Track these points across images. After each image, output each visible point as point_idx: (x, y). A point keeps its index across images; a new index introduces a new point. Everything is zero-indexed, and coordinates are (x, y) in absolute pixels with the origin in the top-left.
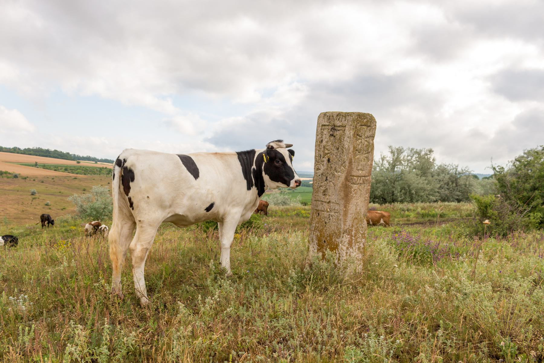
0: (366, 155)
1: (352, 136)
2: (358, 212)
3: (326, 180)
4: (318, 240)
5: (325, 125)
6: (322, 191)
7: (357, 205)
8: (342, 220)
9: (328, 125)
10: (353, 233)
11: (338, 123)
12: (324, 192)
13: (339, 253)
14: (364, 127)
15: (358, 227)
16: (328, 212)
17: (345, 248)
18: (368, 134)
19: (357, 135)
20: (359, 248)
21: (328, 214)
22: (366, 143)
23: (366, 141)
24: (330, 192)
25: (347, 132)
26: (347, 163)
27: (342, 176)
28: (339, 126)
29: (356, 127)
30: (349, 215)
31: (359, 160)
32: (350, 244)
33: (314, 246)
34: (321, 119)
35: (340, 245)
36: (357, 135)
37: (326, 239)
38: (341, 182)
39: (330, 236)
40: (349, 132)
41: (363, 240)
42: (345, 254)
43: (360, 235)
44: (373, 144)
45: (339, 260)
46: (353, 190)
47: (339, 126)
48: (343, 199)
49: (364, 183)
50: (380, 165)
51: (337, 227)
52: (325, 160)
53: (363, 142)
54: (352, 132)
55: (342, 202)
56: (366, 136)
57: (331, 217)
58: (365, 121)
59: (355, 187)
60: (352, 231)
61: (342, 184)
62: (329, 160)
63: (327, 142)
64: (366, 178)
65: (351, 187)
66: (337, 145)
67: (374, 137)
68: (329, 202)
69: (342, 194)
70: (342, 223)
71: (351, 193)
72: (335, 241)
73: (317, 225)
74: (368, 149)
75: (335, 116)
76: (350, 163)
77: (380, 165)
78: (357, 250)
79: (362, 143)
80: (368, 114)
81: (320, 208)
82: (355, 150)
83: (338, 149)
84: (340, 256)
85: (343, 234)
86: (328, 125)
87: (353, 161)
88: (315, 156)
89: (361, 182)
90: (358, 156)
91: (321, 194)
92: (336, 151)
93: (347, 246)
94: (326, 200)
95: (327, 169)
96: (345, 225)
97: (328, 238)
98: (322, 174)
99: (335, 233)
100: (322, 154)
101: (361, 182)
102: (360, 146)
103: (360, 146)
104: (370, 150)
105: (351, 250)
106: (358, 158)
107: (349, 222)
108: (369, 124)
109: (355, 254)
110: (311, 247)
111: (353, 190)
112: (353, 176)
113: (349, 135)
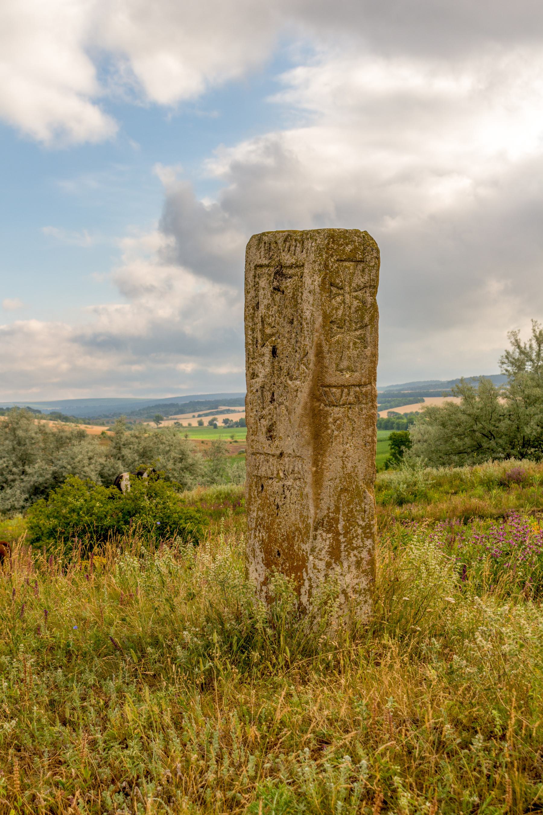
0: (358, 333)
1: (318, 290)
2: (349, 475)
3: (272, 400)
4: (266, 552)
5: (261, 266)
6: (264, 430)
7: (344, 458)
8: (311, 496)
9: (268, 266)
10: (340, 527)
11: (287, 259)
12: (269, 430)
13: (310, 579)
14: (347, 264)
15: (351, 511)
16: (281, 479)
17: (321, 565)
18: (359, 280)
19: (332, 285)
20: (358, 563)
21: (281, 483)
22: (356, 303)
23: (356, 298)
24: (281, 429)
25: (307, 280)
26: (312, 357)
27: (303, 387)
28: (291, 267)
29: (326, 266)
30: (326, 483)
31: (342, 347)
32: (335, 554)
33: (258, 567)
34: (253, 250)
35: (311, 558)
36: (330, 285)
37: (281, 546)
38: (302, 404)
39: (289, 539)
40: (312, 281)
41: (368, 542)
42: (322, 579)
43: (360, 531)
44: (374, 306)
45: (310, 595)
46: (330, 420)
47: (291, 267)
48: (309, 444)
49: (360, 403)
50: (534, 356)
51: (301, 516)
52: (267, 350)
53: (347, 301)
54: (318, 279)
55: (308, 453)
56: (354, 285)
57: (287, 493)
58: (349, 248)
59: (337, 412)
60: (337, 521)
61: (305, 408)
62: (274, 352)
63: (268, 307)
64: (364, 390)
65: (327, 415)
66: (288, 312)
67: (375, 287)
68: (281, 454)
69: (307, 432)
70: (311, 503)
71: (327, 428)
72: (299, 549)
73: (261, 514)
74: (362, 318)
75: (280, 242)
76: (319, 354)
77: (534, 356)
78: (353, 569)
79: (346, 302)
80: (356, 232)
81: (262, 472)
82: (329, 321)
83: (292, 322)
84: (311, 587)
85: (316, 529)
86: (268, 266)
87: (326, 349)
88: (247, 344)
89: (351, 399)
90: (336, 338)
91: (262, 437)
92: (288, 328)
93: (327, 559)
94: (273, 451)
95: (272, 374)
96: (317, 507)
97: (285, 545)
98: (263, 387)
99: (298, 529)
100: (259, 335)
101: (351, 399)
102: (340, 312)
103: (340, 312)
104: (367, 319)
105: (338, 569)
106: (338, 342)
107: (328, 501)
108: (359, 256)
109: (348, 577)
110: (251, 569)
111: (330, 420)
112: (329, 386)
113: (312, 287)
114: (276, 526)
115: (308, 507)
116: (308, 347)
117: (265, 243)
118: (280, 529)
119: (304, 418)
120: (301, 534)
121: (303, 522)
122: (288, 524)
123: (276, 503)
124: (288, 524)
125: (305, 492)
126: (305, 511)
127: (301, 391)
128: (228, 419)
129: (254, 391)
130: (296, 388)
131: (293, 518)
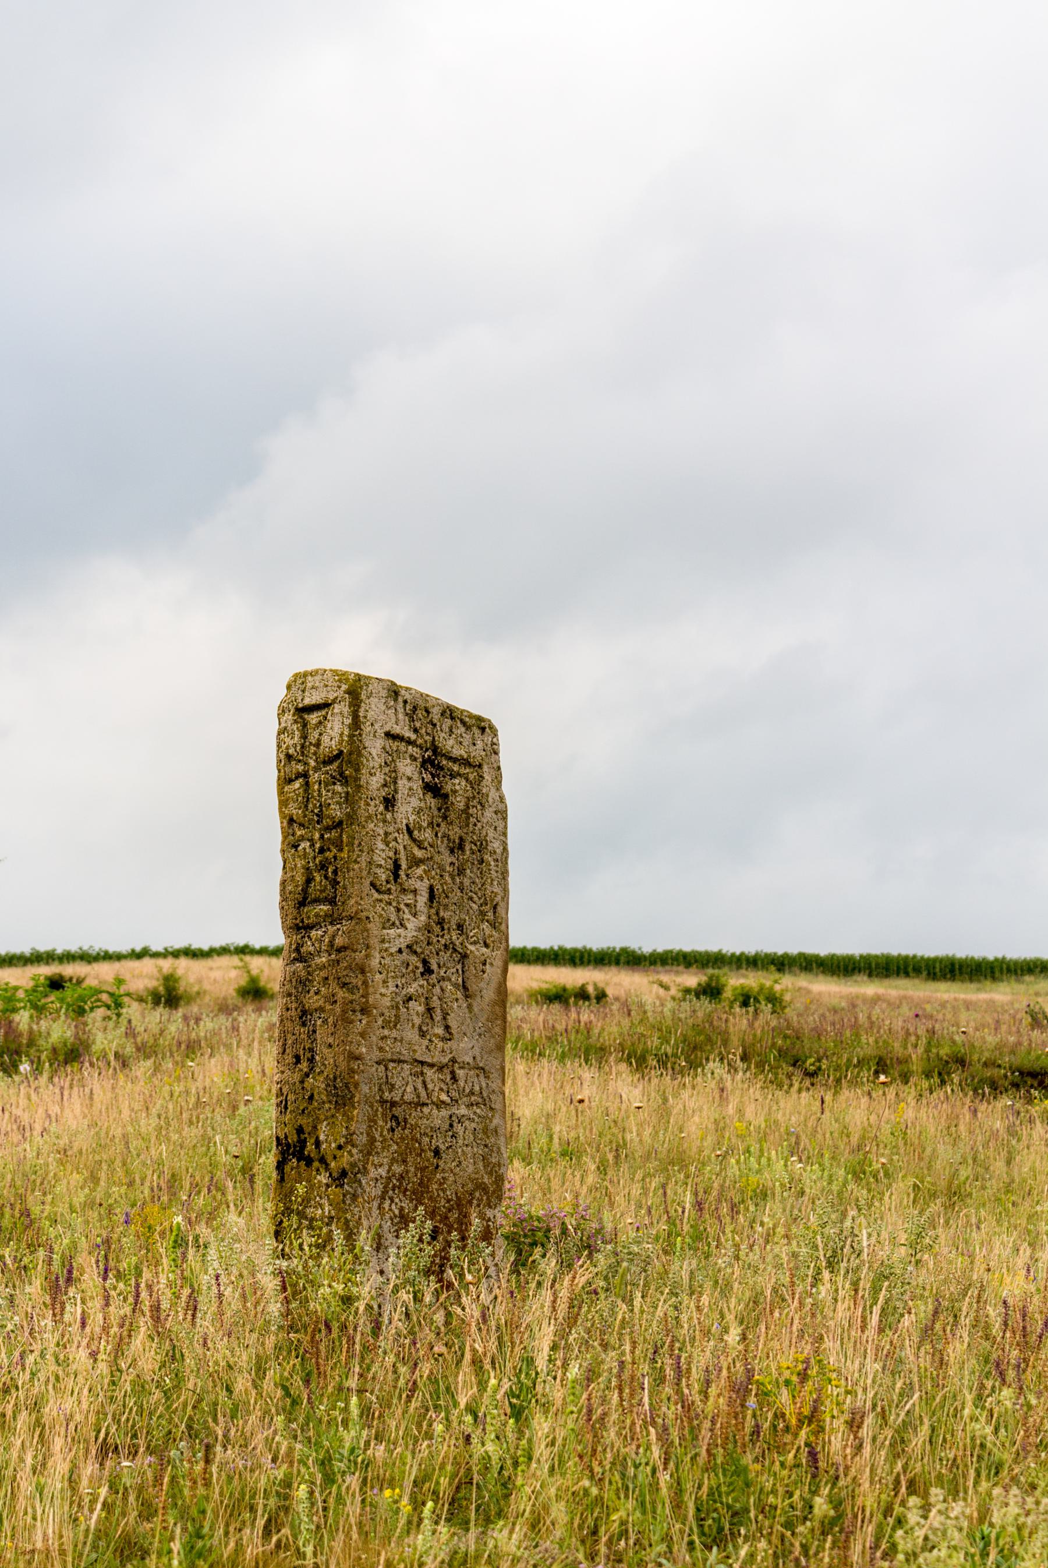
21: (444, 1113)
57: (459, 1128)
114: (435, 1186)
115: (499, 1148)
116: (499, 897)
117: (405, 702)
118: (444, 1191)
119: (497, 1008)
120: (486, 1193)
121: (490, 1173)
122: (460, 1181)
123: (433, 1148)
124: (460, 1181)
125: (492, 1126)
126: (494, 1155)
127: (491, 964)
128: (61, 977)
129: (393, 950)
130: (483, 958)
131: (471, 1168)
